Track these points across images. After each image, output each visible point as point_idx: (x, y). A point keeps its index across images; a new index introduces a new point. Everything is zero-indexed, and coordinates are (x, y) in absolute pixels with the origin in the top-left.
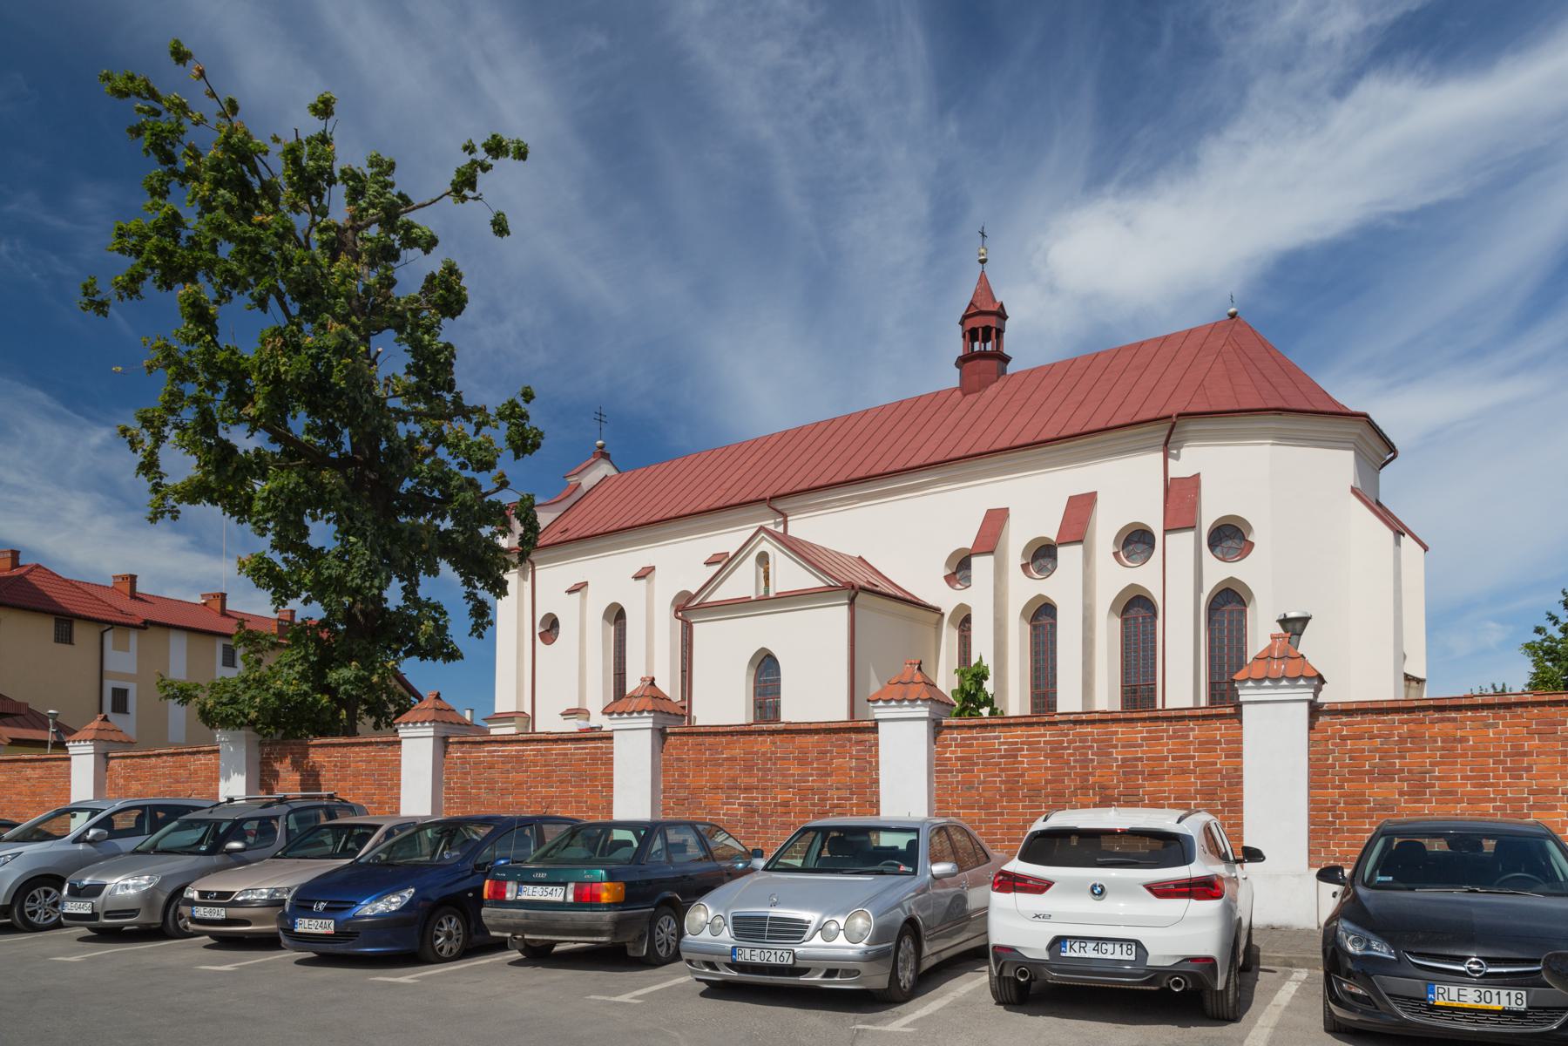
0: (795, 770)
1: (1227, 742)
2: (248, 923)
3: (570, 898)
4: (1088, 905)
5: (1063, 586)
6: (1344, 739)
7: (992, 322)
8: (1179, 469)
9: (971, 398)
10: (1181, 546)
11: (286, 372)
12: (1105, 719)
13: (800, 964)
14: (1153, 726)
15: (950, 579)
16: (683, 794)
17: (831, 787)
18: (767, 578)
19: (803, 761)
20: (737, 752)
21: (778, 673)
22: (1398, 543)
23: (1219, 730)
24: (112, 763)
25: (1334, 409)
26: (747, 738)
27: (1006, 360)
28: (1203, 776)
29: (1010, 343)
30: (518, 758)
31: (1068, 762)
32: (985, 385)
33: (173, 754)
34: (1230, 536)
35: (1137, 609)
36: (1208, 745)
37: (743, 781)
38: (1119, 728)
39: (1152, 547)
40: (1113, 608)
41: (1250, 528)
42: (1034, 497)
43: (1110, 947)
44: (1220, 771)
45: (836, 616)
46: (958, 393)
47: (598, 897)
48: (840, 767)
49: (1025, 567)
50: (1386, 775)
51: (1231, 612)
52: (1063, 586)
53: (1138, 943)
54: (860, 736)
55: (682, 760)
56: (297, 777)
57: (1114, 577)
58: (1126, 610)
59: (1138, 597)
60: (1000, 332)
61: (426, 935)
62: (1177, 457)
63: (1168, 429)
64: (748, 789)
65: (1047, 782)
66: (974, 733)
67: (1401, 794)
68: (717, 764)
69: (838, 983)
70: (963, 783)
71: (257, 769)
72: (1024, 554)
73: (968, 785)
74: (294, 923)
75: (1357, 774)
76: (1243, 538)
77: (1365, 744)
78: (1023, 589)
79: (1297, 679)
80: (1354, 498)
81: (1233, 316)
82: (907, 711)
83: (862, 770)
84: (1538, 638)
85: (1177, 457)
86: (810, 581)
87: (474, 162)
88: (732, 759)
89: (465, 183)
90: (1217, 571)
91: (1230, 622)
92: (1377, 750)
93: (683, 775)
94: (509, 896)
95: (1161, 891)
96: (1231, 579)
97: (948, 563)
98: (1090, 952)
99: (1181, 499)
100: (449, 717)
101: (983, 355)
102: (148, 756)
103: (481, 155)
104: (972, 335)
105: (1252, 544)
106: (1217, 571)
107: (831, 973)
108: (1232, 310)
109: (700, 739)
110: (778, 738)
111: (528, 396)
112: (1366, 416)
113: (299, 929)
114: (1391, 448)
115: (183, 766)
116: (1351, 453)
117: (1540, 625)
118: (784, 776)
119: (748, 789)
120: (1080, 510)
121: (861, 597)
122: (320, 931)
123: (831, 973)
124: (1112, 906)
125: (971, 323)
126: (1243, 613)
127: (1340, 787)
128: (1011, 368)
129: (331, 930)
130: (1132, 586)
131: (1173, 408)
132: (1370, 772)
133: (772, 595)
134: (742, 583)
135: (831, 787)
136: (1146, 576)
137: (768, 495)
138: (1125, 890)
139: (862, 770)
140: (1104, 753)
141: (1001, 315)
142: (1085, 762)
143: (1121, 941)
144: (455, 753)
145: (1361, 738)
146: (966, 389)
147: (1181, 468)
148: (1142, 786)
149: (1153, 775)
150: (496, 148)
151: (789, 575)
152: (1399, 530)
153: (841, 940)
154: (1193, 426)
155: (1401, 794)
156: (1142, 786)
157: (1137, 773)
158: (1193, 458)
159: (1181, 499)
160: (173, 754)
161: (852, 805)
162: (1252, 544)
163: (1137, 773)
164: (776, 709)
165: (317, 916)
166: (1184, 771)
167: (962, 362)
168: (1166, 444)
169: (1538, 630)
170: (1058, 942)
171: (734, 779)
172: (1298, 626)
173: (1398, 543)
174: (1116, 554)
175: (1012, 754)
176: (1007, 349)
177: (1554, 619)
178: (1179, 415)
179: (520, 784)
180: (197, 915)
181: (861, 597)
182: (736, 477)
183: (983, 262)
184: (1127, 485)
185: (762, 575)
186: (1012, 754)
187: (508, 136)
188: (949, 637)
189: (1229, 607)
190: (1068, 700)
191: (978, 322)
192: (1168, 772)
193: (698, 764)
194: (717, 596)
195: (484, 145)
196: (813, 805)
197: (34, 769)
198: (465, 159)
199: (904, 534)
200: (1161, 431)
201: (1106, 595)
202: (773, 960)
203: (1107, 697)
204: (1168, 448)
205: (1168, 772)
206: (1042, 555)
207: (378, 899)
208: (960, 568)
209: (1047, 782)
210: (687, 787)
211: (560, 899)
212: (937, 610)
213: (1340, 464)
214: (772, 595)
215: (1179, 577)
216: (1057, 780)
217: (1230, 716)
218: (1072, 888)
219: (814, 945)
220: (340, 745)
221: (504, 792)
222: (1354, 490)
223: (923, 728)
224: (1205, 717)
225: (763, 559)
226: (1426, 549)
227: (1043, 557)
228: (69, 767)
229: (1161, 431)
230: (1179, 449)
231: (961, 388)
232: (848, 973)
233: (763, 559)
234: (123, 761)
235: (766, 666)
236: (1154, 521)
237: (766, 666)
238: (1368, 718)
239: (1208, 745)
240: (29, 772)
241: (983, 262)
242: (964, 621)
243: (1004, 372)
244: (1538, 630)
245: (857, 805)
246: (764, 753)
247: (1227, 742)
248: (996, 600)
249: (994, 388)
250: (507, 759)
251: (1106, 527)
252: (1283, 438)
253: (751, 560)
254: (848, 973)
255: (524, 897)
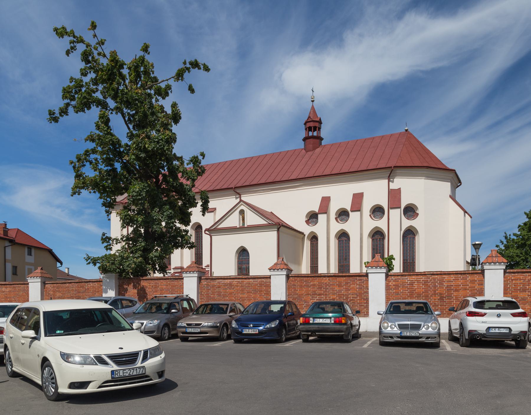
0: (337, 288)
1: (479, 281)
2: (207, 333)
3: (333, 322)
4: (496, 319)
5: (351, 226)
6: (512, 280)
7: (317, 125)
8: (393, 186)
9: (310, 153)
10: (396, 214)
11: (148, 147)
12: (334, 276)
13: (420, 336)
14: (456, 276)
15: (307, 222)
16: (296, 296)
17: (350, 294)
18: (243, 220)
19: (340, 285)
20: (316, 282)
21: (249, 256)
22: (465, 216)
23: (476, 277)
24: (46, 286)
25: (445, 168)
26: (319, 278)
27: (322, 139)
28: (471, 291)
29: (323, 133)
30: (230, 284)
31: (430, 286)
32: (314, 149)
33: (77, 282)
34: (410, 211)
35: (378, 237)
36: (473, 281)
37: (318, 292)
38: (446, 276)
39: (384, 213)
40: (369, 235)
41: (417, 208)
42: (341, 194)
43: (502, 329)
44: (476, 289)
45: (272, 236)
46: (304, 151)
47: (341, 321)
48: (353, 288)
49: (336, 219)
50: (524, 290)
51: (410, 238)
52: (351, 226)
53: (510, 328)
54: (360, 278)
55: (295, 285)
56: (136, 291)
57: (370, 224)
58: (373, 236)
59: (378, 231)
60: (319, 129)
61: (280, 334)
62: (393, 182)
63: (390, 172)
64: (320, 295)
65: (423, 292)
66: (399, 277)
67: (528, 296)
68: (308, 286)
69: (430, 341)
70: (396, 293)
71: (118, 288)
72: (336, 214)
73: (397, 293)
74: (242, 331)
75: (516, 290)
76: (414, 212)
77: (518, 282)
78: (336, 227)
79: (501, 263)
80: (450, 199)
81: (406, 130)
82: (378, 270)
83: (361, 288)
84: (497, 249)
85: (393, 182)
86: (261, 221)
87: (185, 67)
88: (314, 285)
89: (180, 75)
90: (407, 223)
91: (410, 241)
92: (522, 283)
93: (295, 290)
94: (311, 322)
95: (514, 315)
96: (411, 226)
97: (307, 216)
98: (497, 331)
99: (394, 197)
100: (202, 270)
101: (313, 137)
102: (65, 283)
103: (188, 65)
104: (310, 129)
105: (418, 214)
106: (407, 223)
107: (428, 338)
108: (406, 128)
109: (302, 278)
110: (331, 278)
111: (203, 155)
112: (455, 170)
113: (244, 332)
114: (460, 182)
115: (83, 287)
116: (450, 183)
117: (498, 244)
118: (333, 290)
119: (320, 295)
120: (357, 200)
121: (282, 229)
122: (253, 333)
123: (428, 338)
124: (501, 319)
125: (309, 125)
126: (414, 238)
127: (511, 294)
128: (323, 143)
129: (257, 332)
130: (376, 227)
131: (392, 164)
132: (520, 290)
133: (246, 226)
134: (234, 221)
135: (350, 294)
136: (382, 224)
137: (232, 186)
138: (506, 315)
139: (361, 288)
140: (441, 284)
141: (320, 122)
142: (435, 286)
143: (505, 328)
144: (204, 282)
145: (517, 280)
146: (306, 149)
147: (394, 186)
148: (453, 294)
149: (456, 290)
150: (195, 65)
151: (252, 219)
152: (465, 212)
153: (430, 329)
154: (398, 171)
155: (528, 296)
156: (453, 294)
157: (452, 290)
158: (398, 183)
159: (394, 197)
160: (77, 282)
161: (357, 300)
162: (418, 214)
163: (452, 290)
164: (248, 269)
165: (250, 328)
166: (466, 289)
167: (305, 139)
168: (389, 177)
169: (497, 246)
170: (489, 328)
171: (315, 291)
172: (478, 246)
173: (465, 216)
174: (370, 215)
175: (412, 284)
176: (322, 135)
177: (502, 242)
178: (394, 167)
179: (231, 293)
180: (188, 331)
181: (282, 229)
182: (215, 178)
183: (313, 101)
184: (375, 191)
185: (241, 218)
186: (412, 284)
187: (201, 61)
188: (307, 244)
189: (410, 236)
190: (322, 269)
191: (311, 124)
192: (461, 289)
193: (301, 286)
194: (222, 226)
195: (190, 62)
196: (344, 300)
197: (6, 288)
198: (183, 66)
199: (292, 204)
200: (388, 172)
201: (367, 231)
202: (413, 335)
203: (334, 269)
204: (390, 178)
205: (461, 289)
206: (343, 214)
207: (268, 324)
208: (312, 218)
209: (423, 292)
210: (297, 294)
211: (329, 322)
212: (302, 233)
213: (446, 187)
214: (246, 226)
215: (395, 224)
216: (426, 291)
217: (480, 273)
218: (492, 315)
219: (423, 330)
220: (18, 284)
221: (225, 296)
222: (450, 196)
223: (384, 275)
224: (472, 273)
225: (242, 212)
226: (471, 217)
227: (343, 215)
228: (28, 287)
229: (388, 171)
230: (393, 179)
231: (305, 149)
232: (432, 338)
233: (242, 212)
234: (52, 285)
235: (243, 254)
236: (385, 205)
237: (243, 254)
238: (519, 274)
239: (473, 281)
240: (4, 289)
241: (313, 101)
242: (314, 238)
243: (321, 144)
244: (497, 246)
245: (359, 300)
246: (326, 283)
247: (479, 281)
248: (326, 229)
249: (318, 150)
250: (225, 285)
251: (367, 205)
252: (428, 177)
253: (237, 213)
254: (432, 338)
255: (316, 322)
